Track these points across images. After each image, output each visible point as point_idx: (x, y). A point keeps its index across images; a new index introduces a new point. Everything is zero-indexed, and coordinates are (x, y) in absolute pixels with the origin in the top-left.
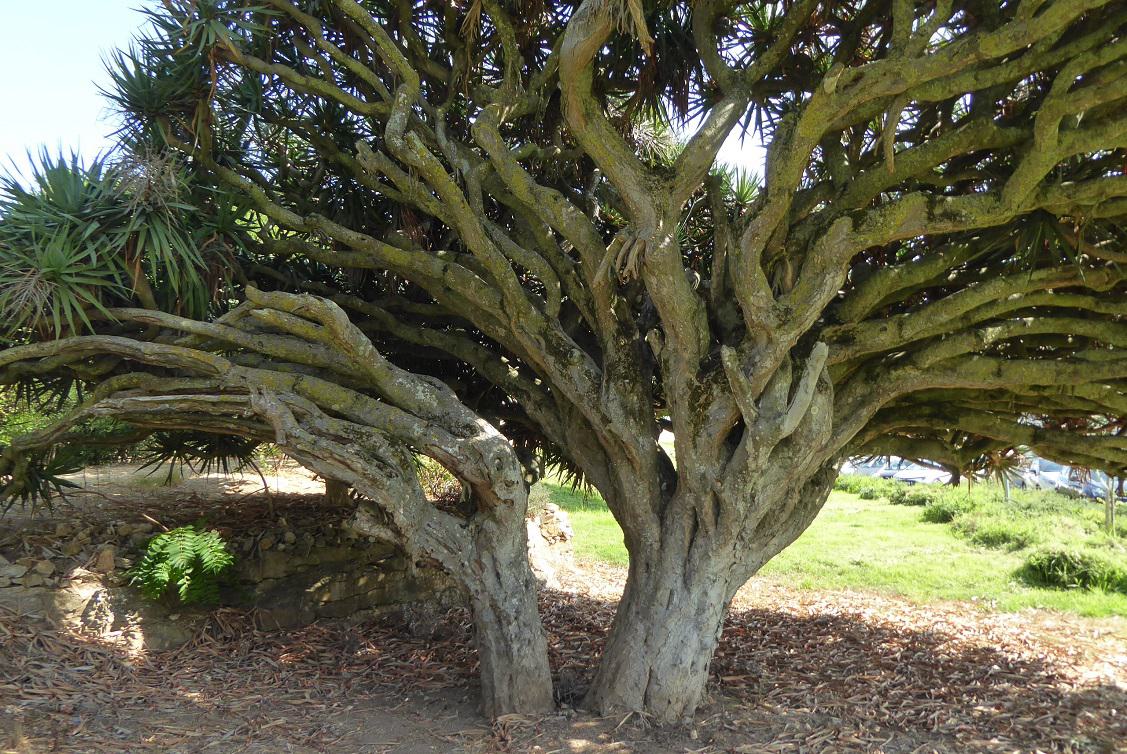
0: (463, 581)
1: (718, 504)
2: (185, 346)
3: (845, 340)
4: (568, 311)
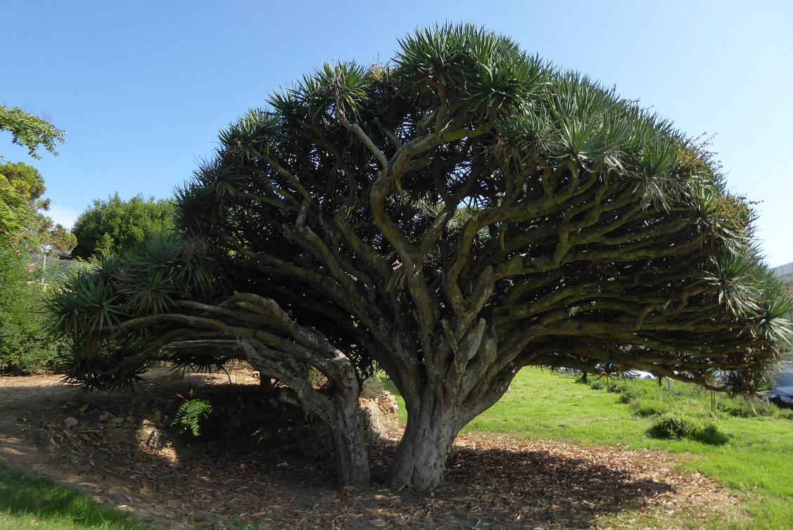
0: (329, 425)
1: (444, 389)
2: (205, 317)
3: (506, 313)
4: (379, 298)
